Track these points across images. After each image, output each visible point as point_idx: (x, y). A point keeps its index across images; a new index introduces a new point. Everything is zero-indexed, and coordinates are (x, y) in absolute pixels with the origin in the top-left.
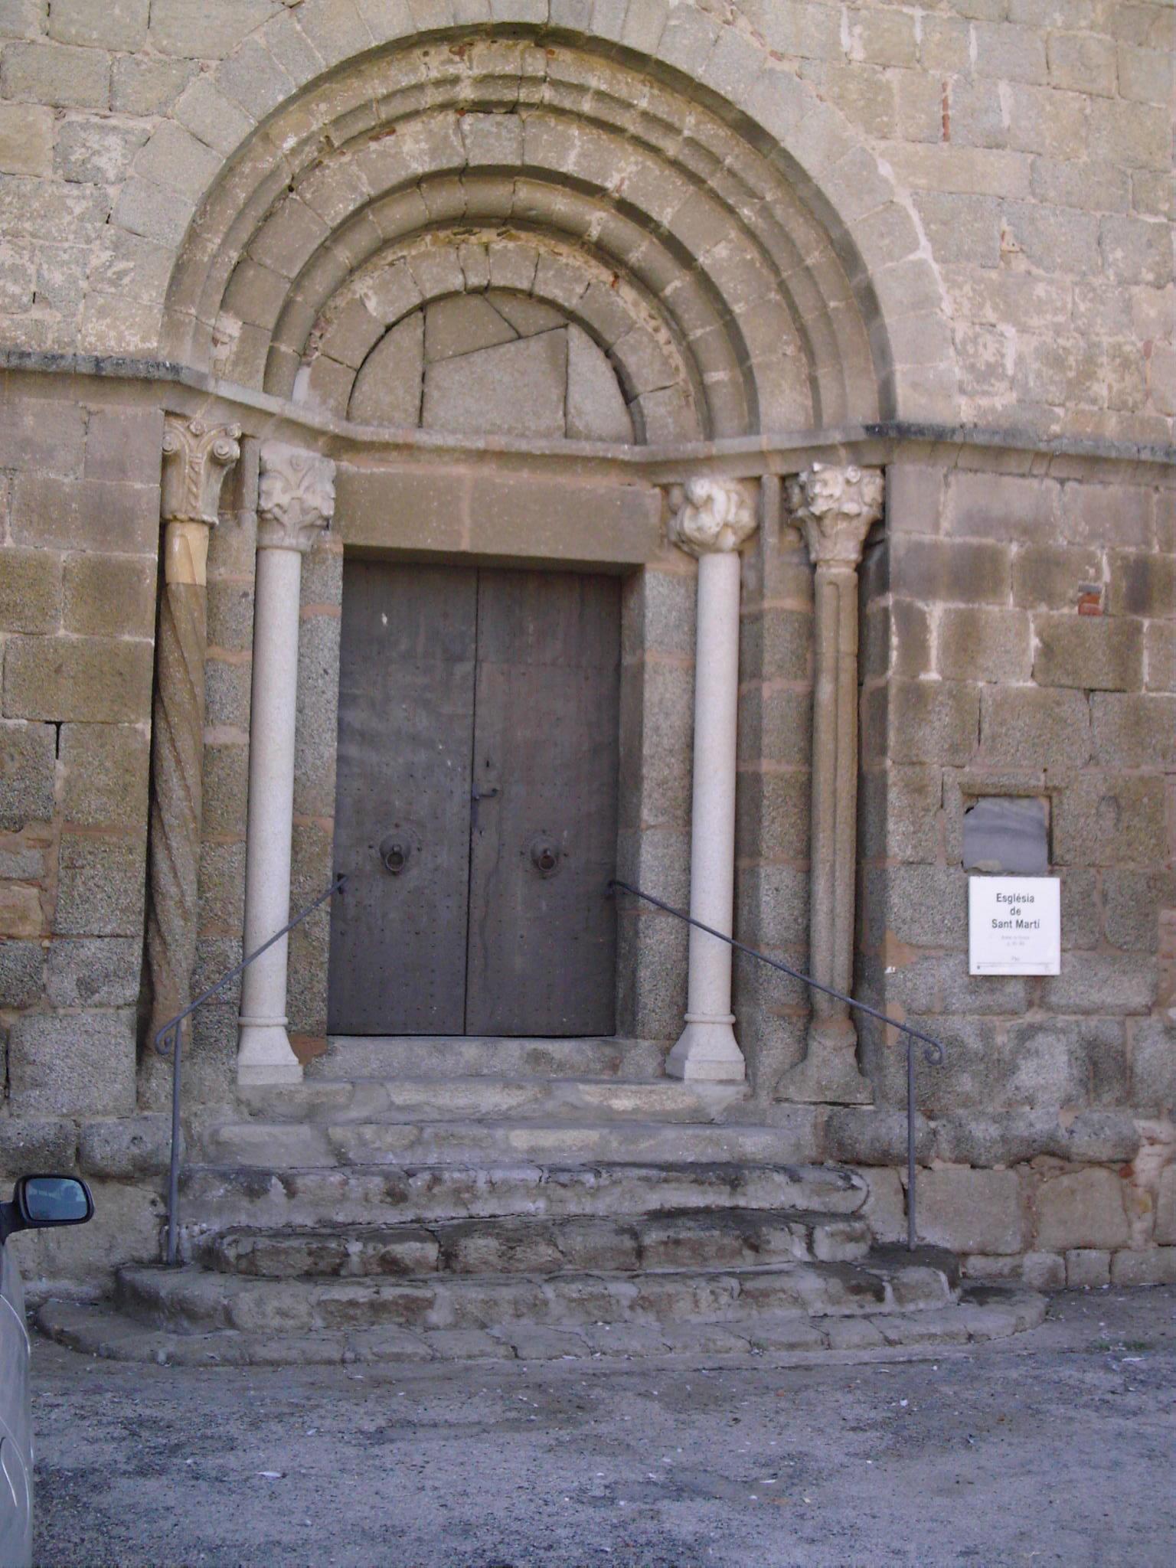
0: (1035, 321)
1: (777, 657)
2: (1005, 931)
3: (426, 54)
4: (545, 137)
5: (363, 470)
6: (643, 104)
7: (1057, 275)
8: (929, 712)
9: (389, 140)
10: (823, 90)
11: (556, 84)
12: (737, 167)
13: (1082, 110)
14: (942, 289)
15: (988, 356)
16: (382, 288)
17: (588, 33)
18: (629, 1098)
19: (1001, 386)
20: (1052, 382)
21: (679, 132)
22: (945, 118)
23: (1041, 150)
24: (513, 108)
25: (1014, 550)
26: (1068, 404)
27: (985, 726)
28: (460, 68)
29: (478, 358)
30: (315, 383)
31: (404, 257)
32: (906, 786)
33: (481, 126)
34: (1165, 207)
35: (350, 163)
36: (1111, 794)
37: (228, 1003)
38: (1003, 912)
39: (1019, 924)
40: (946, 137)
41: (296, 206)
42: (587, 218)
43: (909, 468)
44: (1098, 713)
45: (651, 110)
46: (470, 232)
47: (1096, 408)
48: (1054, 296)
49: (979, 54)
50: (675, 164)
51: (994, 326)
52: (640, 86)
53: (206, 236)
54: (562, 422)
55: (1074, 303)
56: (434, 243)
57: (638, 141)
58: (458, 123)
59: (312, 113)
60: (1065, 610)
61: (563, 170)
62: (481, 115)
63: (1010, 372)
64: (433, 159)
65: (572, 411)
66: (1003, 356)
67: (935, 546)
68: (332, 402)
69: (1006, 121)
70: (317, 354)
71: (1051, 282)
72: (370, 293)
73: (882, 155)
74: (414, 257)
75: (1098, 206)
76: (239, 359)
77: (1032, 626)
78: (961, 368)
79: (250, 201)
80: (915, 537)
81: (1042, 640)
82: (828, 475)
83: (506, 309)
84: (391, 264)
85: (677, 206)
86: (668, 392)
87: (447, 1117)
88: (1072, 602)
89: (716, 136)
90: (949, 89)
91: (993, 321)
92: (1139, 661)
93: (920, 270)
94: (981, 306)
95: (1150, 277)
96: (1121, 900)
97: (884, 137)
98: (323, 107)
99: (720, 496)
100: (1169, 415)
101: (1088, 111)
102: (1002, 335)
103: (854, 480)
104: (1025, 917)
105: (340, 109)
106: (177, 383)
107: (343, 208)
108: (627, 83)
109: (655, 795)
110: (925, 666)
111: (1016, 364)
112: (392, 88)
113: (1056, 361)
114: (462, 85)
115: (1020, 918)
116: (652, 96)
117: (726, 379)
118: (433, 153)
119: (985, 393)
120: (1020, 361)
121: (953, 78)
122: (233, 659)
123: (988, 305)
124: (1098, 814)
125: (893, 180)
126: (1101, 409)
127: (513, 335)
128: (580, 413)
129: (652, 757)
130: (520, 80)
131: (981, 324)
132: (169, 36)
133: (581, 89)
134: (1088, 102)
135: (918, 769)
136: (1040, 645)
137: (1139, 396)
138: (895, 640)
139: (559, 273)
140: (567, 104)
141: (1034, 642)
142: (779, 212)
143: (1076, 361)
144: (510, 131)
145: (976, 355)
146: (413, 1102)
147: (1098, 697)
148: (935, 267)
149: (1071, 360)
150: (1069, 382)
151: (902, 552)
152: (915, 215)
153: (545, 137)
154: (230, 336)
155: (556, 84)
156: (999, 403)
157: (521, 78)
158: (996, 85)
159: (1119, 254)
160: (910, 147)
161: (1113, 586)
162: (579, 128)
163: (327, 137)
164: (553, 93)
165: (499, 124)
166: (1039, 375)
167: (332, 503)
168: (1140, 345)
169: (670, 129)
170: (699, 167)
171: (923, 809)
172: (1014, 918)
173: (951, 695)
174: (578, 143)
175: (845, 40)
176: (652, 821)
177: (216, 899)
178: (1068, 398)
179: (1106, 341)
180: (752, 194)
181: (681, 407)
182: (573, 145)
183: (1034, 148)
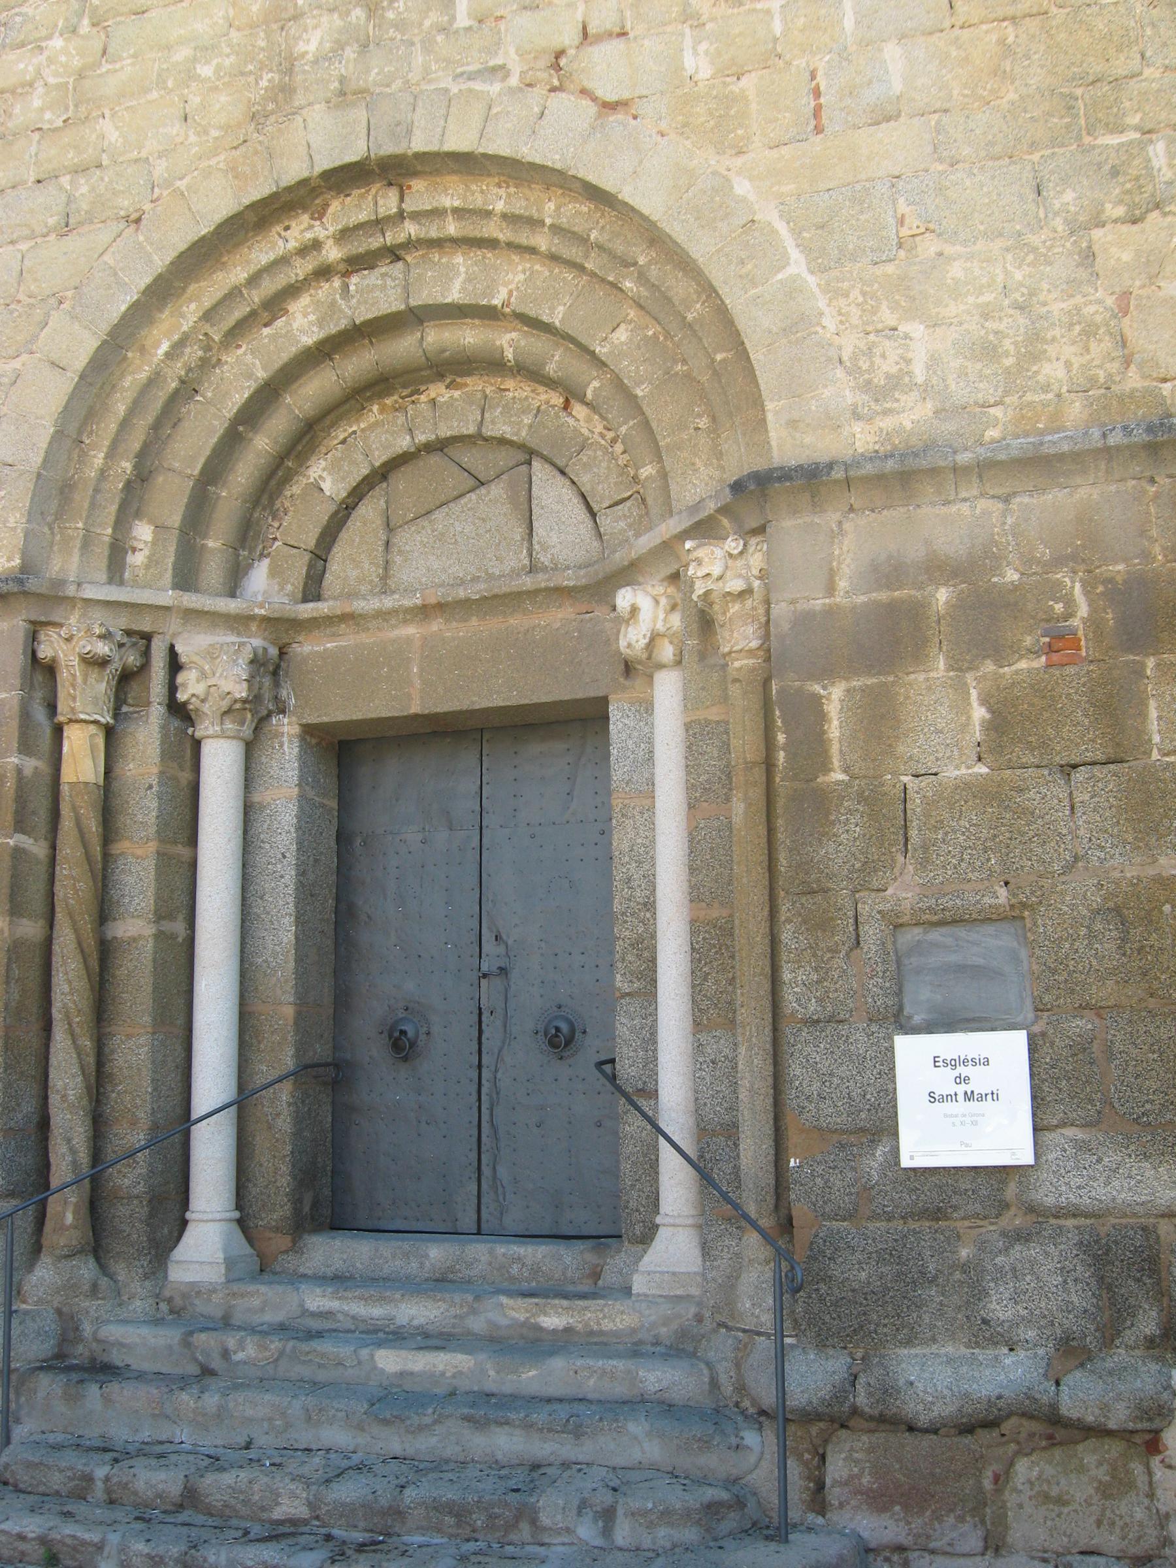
0: (953, 309)
1: (703, 778)
2: (948, 1107)
3: (287, 228)
4: (430, 274)
5: (316, 649)
6: (500, 206)
7: (980, 245)
8: (833, 823)
9: (279, 323)
10: (663, 125)
11: (416, 216)
12: (603, 238)
13: (1002, 42)
14: (822, 304)
15: (889, 366)
16: (334, 468)
17: (410, 153)
18: (559, 1315)
19: (907, 399)
20: (981, 377)
21: (541, 223)
22: (817, 112)
23: (946, 105)
24: (394, 254)
25: (942, 596)
26: (1007, 400)
27: (913, 833)
28: (323, 230)
29: (438, 515)
30: (273, 572)
31: (354, 432)
32: (805, 922)
33: (366, 282)
34: (1135, 119)
35: (245, 354)
36: (1111, 904)
37: (137, 1197)
38: (944, 1081)
39: (969, 1096)
40: (819, 130)
41: (199, 406)
42: (498, 343)
43: (788, 523)
44: (1081, 797)
45: (508, 210)
46: (418, 392)
47: (1050, 396)
48: (977, 272)
49: (857, 23)
50: (554, 258)
51: (895, 329)
52: (496, 190)
53: (92, 453)
54: (526, 562)
55: (1006, 272)
56: (382, 411)
57: (511, 246)
58: (345, 287)
59: (183, 316)
60: (1023, 665)
61: (448, 300)
62: (366, 272)
63: (920, 379)
64: (321, 327)
65: (536, 547)
66: (908, 362)
67: (830, 612)
68: (289, 587)
69: (897, 87)
70: (277, 544)
71: (970, 257)
72: (325, 474)
73: (739, 174)
74: (363, 430)
75: (1033, 146)
76: (152, 562)
77: (974, 693)
78: (853, 389)
79: (132, 411)
80: (802, 606)
81: (990, 710)
82: (701, 553)
83: (465, 460)
84: (343, 442)
85: (568, 300)
86: (628, 503)
87: (362, 1327)
88: (1034, 653)
89: (578, 213)
90: (820, 74)
91: (893, 323)
92: (1143, 715)
93: (793, 289)
94: (874, 311)
95: (1120, 211)
96: (1134, 1052)
97: (740, 153)
98: (193, 306)
99: (645, 603)
100: (1165, 380)
101: (1011, 39)
102: (907, 337)
103: (736, 552)
104: (976, 1086)
105: (207, 304)
106: (25, 593)
107: (238, 397)
108: (482, 192)
109: (630, 958)
110: (826, 768)
111: (928, 368)
112: (253, 269)
113: (988, 351)
114: (327, 247)
115: (969, 1089)
116: (509, 195)
117: (654, 472)
118: (320, 323)
119: (886, 412)
120: (934, 362)
121: (821, 63)
122: (139, 852)
123: (884, 307)
124: (1092, 936)
125: (752, 197)
126: (1059, 396)
127: (471, 482)
128: (545, 548)
129: (623, 914)
130: (378, 224)
131: (878, 331)
132: (35, 280)
133: (437, 213)
134: (1010, 29)
135: (819, 898)
136: (988, 716)
137: (1114, 367)
138: (781, 738)
139: (507, 409)
140: (434, 234)
141: (979, 713)
142: (654, 273)
143: (1015, 344)
144: (394, 280)
145: (872, 369)
146: (327, 1308)
147: (1080, 775)
148: (812, 280)
149: (1008, 344)
150: (1007, 371)
151: (786, 627)
152: (782, 228)
153: (430, 274)
154: (145, 542)
155: (416, 216)
156: (906, 422)
157: (378, 222)
158: (880, 50)
159: (1069, 196)
160: (774, 154)
161: (1094, 623)
162: (464, 254)
163: (206, 334)
164: (417, 227)
165: (384, 275)
166: (962, 373)
167: (245, 685)
168: (1110, 301)
169: (535, 223)
170: (572, 252)
171: (830, 950)
172: (961, 1089)
173: (861, 798)
174: (462, 269)
175: (689, 62)
176: (626, 988)
177: (125, 1092)
178: (1007, 393)
179: (1057, 308)
180: (627, 264)
181: (641, 516)
182: (458, 273)
183: (938, 105)
